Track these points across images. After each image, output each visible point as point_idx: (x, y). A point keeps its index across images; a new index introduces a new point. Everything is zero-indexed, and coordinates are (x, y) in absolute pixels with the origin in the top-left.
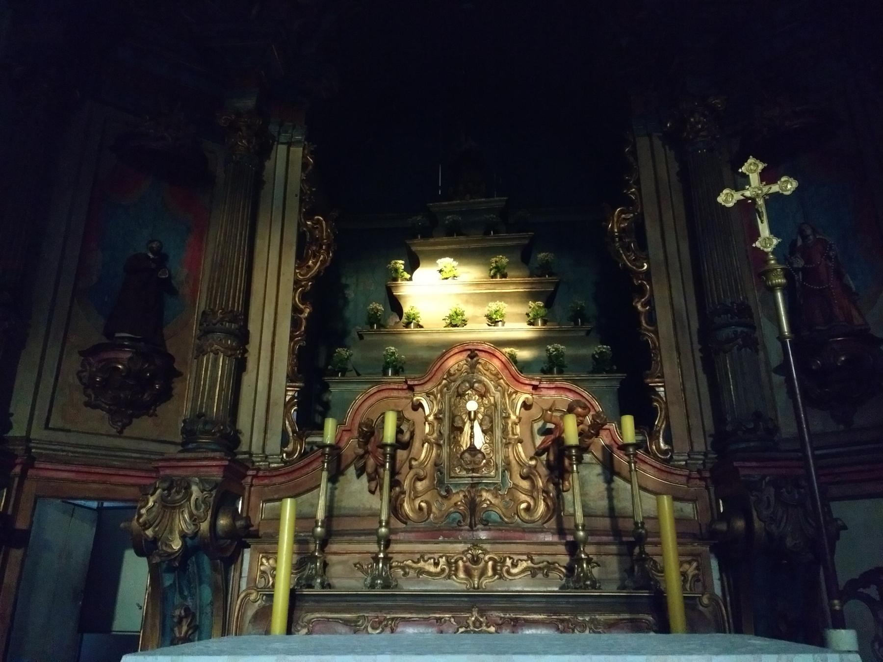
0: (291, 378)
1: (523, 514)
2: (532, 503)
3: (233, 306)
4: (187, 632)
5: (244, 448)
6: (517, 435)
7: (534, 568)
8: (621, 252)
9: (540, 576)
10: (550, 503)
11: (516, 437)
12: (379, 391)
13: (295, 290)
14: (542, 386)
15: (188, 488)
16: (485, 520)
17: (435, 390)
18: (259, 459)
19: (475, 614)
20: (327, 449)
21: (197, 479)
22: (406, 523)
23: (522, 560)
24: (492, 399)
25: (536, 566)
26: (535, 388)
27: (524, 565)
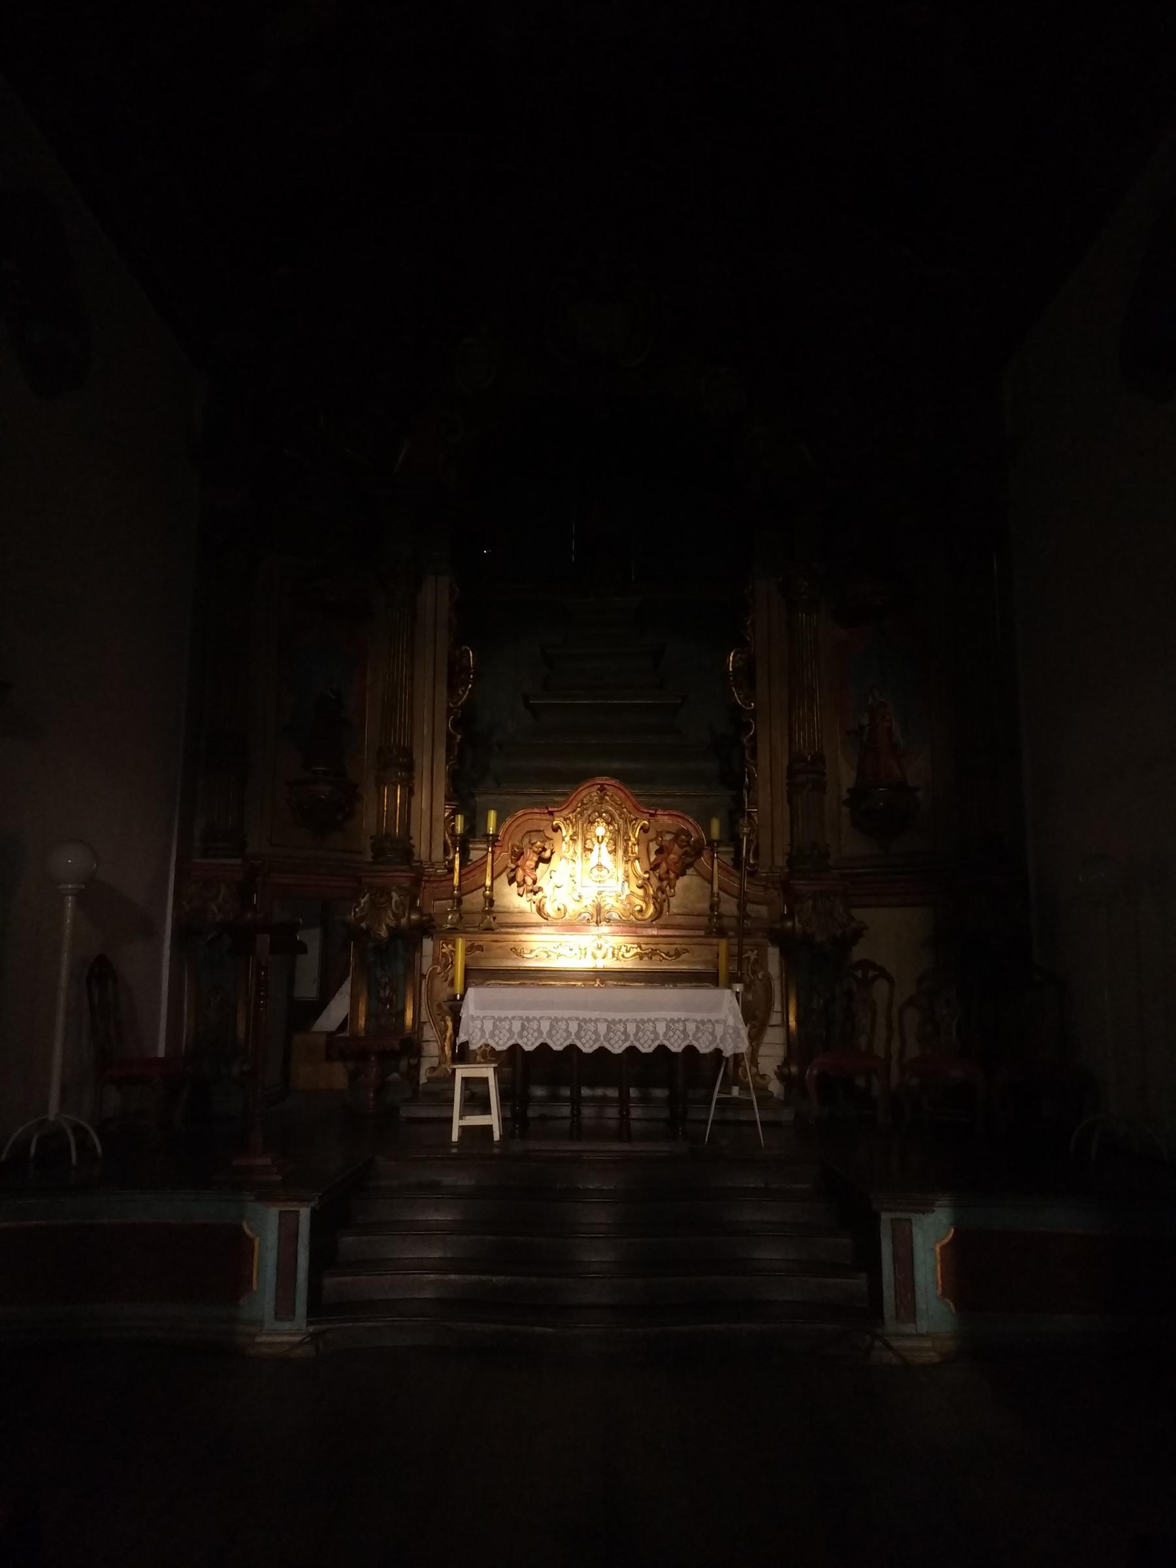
0: (448, 799)
1: (636, 914)
2: (644, 906)
3: (404, 743)
4: (389, 994)
5: (416, 858)
6: (635, 853)
7: (641, 953)
8: (734, 690)
9: (646, 958)
10: (657, 906)
11: (634, 855)
12: (524, 815)
13: (448, 717)
14: (658, 813)
15: (390, 894)
16: (608, 919)
17: (571, 815)
18: (427, 866)
19: (598, 982)
20: (458, 837)
21: (395, 888)
22: (547, 919)
23: (633, 948)
24: (616, 825)
25: (643, 952)
26: (652, 815)
27: (635, 951)
